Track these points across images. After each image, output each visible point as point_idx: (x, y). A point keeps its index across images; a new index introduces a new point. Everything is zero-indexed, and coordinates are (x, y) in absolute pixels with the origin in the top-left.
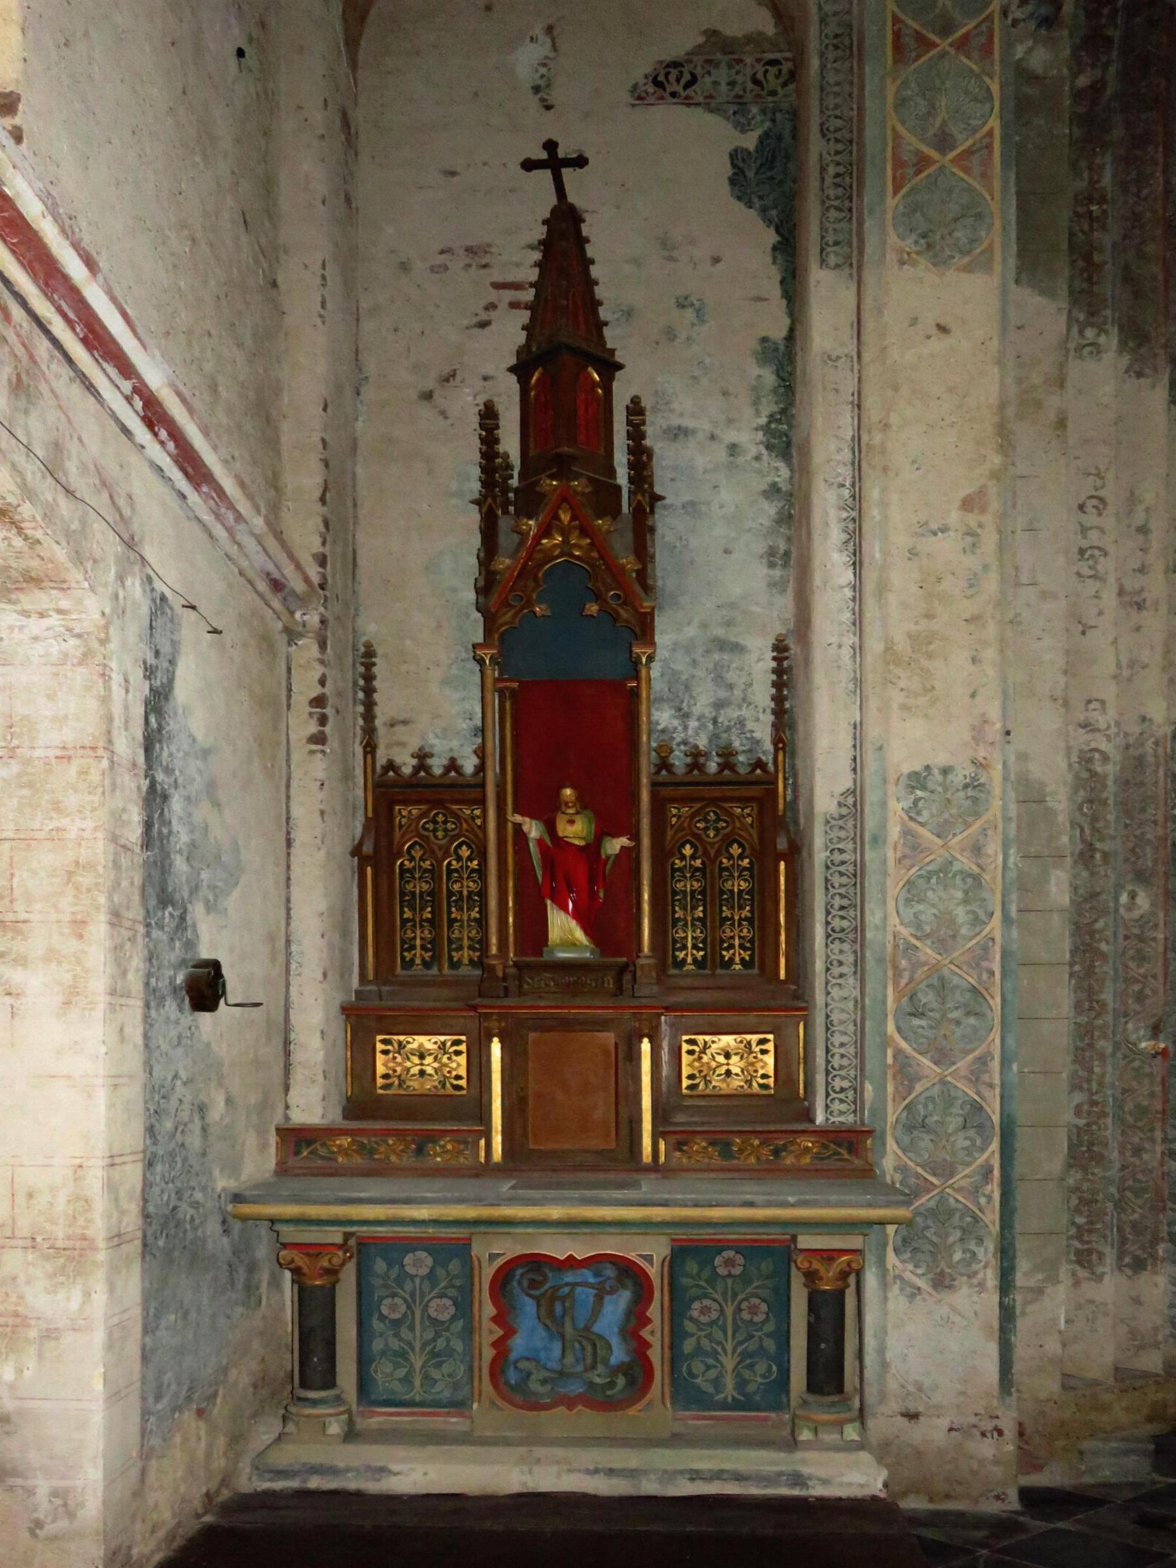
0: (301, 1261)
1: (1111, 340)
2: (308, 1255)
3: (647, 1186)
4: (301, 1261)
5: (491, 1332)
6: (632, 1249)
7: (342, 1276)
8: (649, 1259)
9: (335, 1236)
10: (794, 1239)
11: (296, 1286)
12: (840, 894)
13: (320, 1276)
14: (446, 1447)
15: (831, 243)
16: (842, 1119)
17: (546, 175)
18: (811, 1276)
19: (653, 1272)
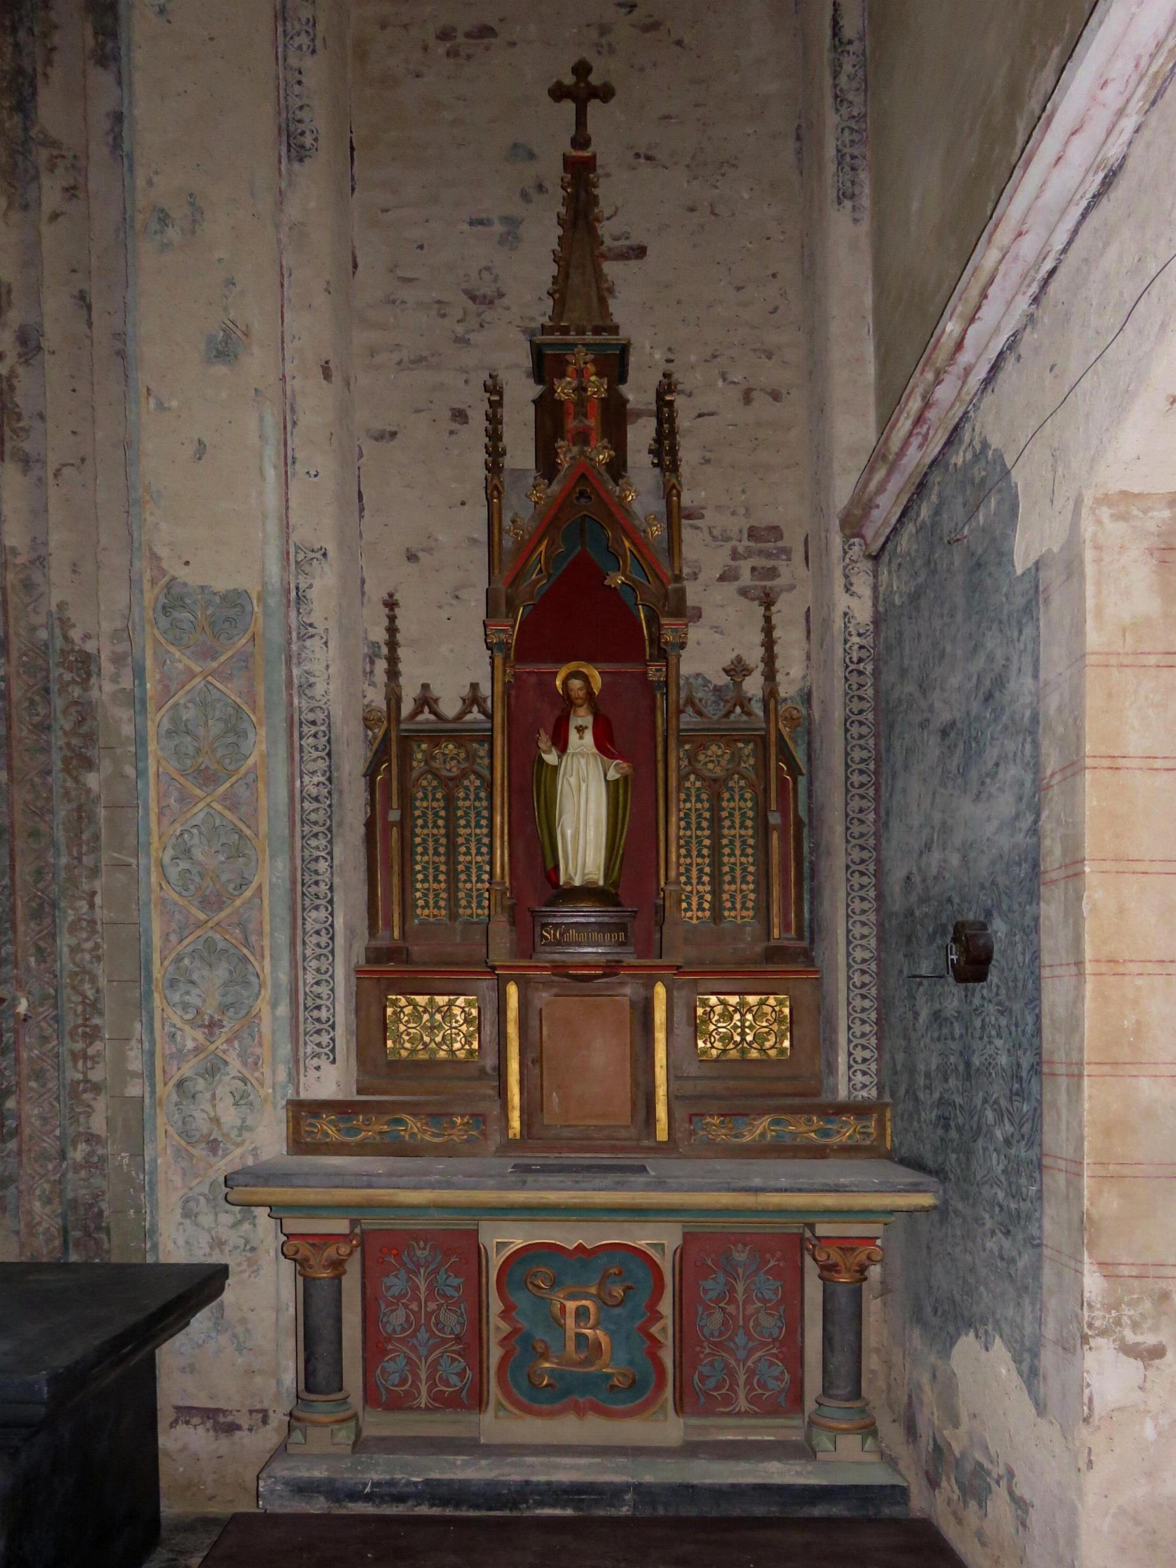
0: (305, 1250)
1: (989, 931)
2: (313, 1245)
3: (655, 1166)
4: (305, 1250)
5: (498, 1328)
6: (642, 1237)
7: (347, 1266)
8: (660, 1247)
9: (340, 1226)
10: (811, 1227)
11: (300, 1280)
12: (861, 946)
13: (325, 1267)
14: (708, 1481)
15: (857, 911)
16: (864, 1093)
17: (569, 107)
18: (828, 1270)
19: (666, 1267)
